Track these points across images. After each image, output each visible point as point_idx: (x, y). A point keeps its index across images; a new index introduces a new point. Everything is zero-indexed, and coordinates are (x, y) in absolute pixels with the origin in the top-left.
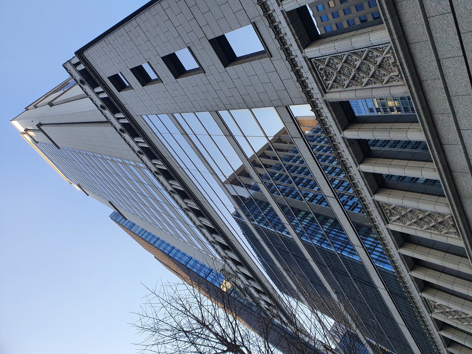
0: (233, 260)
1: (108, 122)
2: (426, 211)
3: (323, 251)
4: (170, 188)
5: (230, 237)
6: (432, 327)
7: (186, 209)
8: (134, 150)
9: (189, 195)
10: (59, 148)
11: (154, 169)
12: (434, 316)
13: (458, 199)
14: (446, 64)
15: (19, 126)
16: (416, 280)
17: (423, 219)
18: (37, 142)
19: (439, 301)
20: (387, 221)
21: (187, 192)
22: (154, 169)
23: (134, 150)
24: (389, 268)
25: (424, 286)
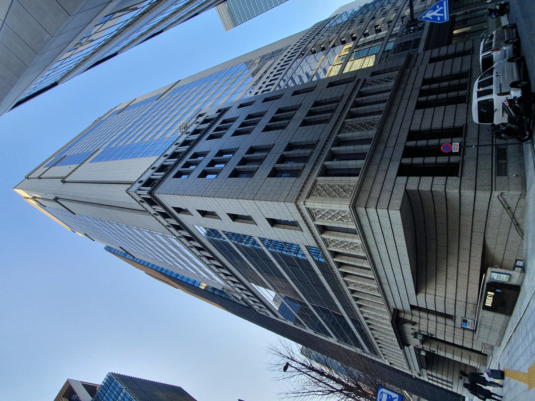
0: (206, 257)
1: (146, 211)
2: (336, 210)
3: (282, 255)
4: (153, 212)
5: (261, 297)
6: (356, 307)
7: (168, 226)
8: (163, 225)
9: (156, 201)
10: (74, 214)
11: (139, 199)
12: (349, 288)
13: (364, 237)
14: (379, 244)
15: (22, 193)
16: (336, 262)
17: (334, 215)
18: (45, 206)
19: (332, 238)
20: (314, 220)
21: (168, 213)
22: (139, 199)
23: (163, 225)
24: (322, 260)
25: (345, 274)
